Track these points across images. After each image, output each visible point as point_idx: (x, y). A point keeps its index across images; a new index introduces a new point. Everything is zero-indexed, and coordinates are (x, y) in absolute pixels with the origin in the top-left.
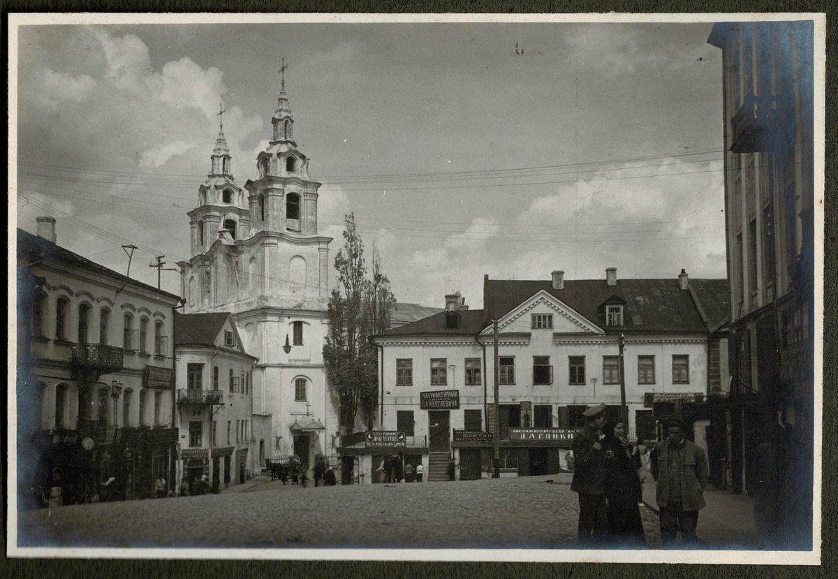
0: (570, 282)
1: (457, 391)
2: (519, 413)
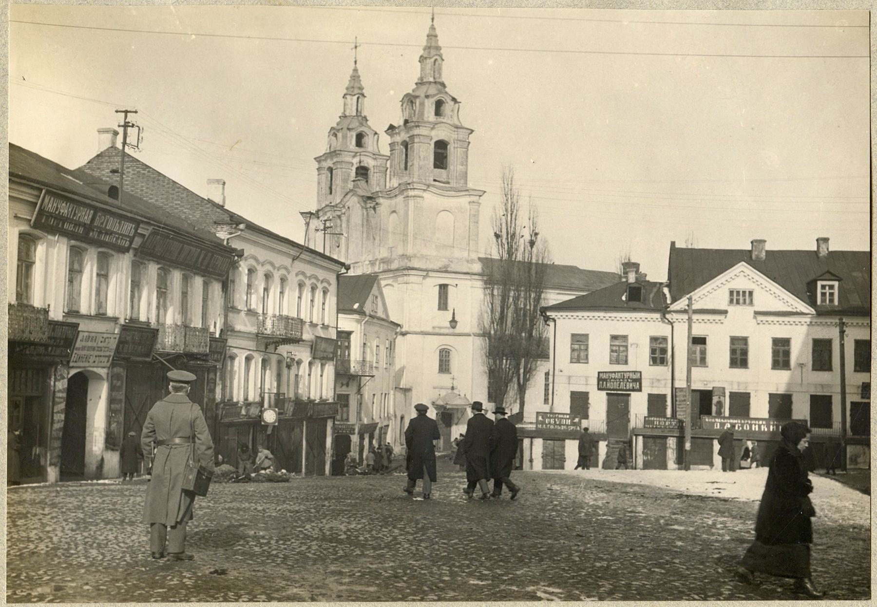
0: (773, 252)
1: (641, 372)
2: (711, 400)
